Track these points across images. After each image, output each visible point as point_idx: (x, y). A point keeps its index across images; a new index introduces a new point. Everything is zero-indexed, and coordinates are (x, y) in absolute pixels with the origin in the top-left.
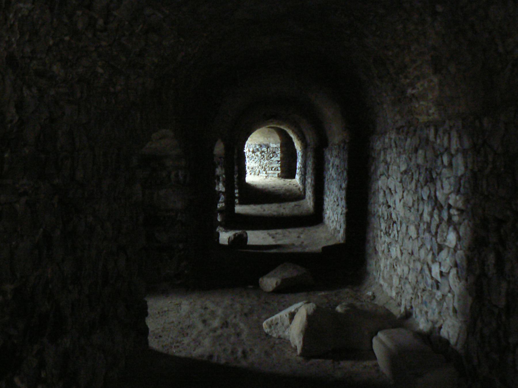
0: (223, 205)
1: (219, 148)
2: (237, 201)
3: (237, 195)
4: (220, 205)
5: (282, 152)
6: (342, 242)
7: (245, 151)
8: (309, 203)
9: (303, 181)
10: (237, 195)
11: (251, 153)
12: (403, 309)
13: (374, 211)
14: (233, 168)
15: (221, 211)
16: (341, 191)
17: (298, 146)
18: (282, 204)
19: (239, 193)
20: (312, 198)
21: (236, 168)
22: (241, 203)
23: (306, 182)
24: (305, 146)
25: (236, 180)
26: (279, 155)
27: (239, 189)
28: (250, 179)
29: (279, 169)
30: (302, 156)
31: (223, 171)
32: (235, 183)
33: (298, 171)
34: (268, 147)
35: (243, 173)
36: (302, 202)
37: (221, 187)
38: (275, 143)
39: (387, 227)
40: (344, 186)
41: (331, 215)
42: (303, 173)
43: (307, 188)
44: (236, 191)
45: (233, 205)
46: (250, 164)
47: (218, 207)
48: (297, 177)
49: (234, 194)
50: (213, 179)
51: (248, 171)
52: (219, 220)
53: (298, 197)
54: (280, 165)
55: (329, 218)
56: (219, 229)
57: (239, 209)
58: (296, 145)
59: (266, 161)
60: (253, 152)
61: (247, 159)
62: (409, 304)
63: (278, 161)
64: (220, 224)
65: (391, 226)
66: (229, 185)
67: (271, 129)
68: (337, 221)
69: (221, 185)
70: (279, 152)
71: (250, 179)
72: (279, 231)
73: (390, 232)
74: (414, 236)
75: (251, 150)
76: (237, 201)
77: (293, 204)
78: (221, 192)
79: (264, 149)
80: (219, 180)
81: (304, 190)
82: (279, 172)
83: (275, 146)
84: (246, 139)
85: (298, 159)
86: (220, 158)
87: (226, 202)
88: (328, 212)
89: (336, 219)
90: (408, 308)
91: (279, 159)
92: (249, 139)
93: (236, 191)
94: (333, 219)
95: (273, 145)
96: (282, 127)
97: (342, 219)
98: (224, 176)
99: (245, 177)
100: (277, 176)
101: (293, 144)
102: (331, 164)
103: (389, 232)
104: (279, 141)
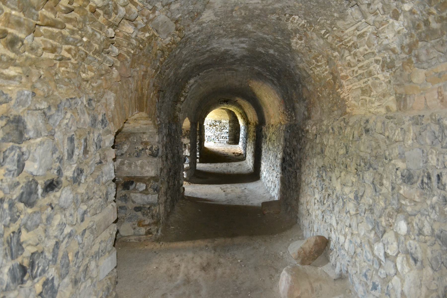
0: (188, 165)
1: (186, 124)
2: (198, 160)
3: (198, 156)
4: (186, 166)
5: (230, 126)
6: (277, 198)
7: (204, 125)
8: (249, 162)
9: (245, 149)
10: (198, 156)
11: (208, 126)
12: (337, 270)
13: (308, 182)
14: (196, 138)
15: (187, 170)
16: (277, 160)
17: (241, 123)
18: (230, 164)
19: (199, 155)
20: (251, 161)
21: (198, 137)
22: (200, 162)
23: (247, 149)
24: (247, 123)
25: (198, 145)
26: (228, 128)
27: (199, 152)
28: (208, 144)
29: (228, 138)
30: (244, 130)
31: (189, 141)
32: (197, 143)
33: (241, 140)
34: (220, 122)
35: (202, 140)
36: (244, 162)
37: (187, 153)
38: (226, 120)
39: (322, 198)
40: (279, 156)
41: (267, 175)
42: (245, 142)
43: (247, 153)
44: (198, 153)
45: (195, 163)
46: (208, 133)
47: (185, 167)
48: (240, 143)
49: (196, 155)
50: (182, 146)
51: (206, 138)
52: (185, 177)
53: (240, 158)
54: (228, 135)
55: (265, 177)
56: (189, 154)
57: (200, 166)
58: (240, 121)
59: (219, 132)
60: (210, 125)
61: (206, 131)
62: (345, 269)
63: (227, 132)
64: (185, 180)
65: (326, 197)
66: (193, 150)
67: (223, 110)
68: (272, 182)
69: (187, 151)
70: (227, 126)
71: (208, 144)
72: (228, 186)
73: (325, 202)
74: (353, 212)
75: (209, 124)
76: (198, 160)
77: (237, 164)
78: (187, 156)
79: (218, 124)
80: (185, 147)
81: (245, 154)
82: (228, 140)
83: (225, 122)
84: (206, 116)
85: (241, 132)
86: (187, 131)
87: (190, 163)
88: (264, 173)
89: (272, 180)
90: (344, 272)
91: (228, 131)
92: (208, 116)
93: (198, 153)
94: (268, 179)
95: (223, 121)
96: (230, 109)
97: (277, 182)
98: (189, 144)
99: (204, 143)
100: (226, 142)
101: (237, 121)
102: (268, 138)
103: (324, 202)
104: (228, 118)
